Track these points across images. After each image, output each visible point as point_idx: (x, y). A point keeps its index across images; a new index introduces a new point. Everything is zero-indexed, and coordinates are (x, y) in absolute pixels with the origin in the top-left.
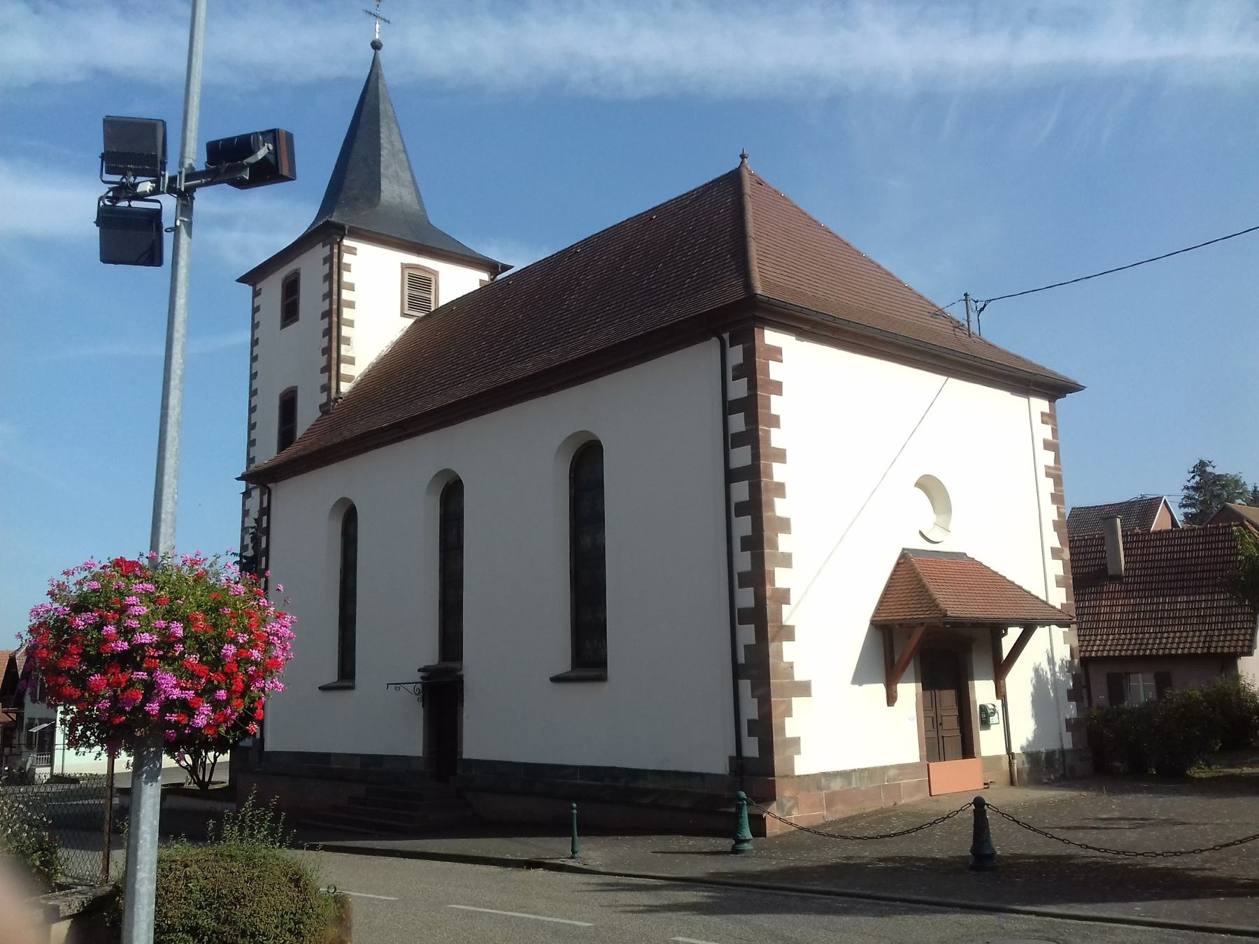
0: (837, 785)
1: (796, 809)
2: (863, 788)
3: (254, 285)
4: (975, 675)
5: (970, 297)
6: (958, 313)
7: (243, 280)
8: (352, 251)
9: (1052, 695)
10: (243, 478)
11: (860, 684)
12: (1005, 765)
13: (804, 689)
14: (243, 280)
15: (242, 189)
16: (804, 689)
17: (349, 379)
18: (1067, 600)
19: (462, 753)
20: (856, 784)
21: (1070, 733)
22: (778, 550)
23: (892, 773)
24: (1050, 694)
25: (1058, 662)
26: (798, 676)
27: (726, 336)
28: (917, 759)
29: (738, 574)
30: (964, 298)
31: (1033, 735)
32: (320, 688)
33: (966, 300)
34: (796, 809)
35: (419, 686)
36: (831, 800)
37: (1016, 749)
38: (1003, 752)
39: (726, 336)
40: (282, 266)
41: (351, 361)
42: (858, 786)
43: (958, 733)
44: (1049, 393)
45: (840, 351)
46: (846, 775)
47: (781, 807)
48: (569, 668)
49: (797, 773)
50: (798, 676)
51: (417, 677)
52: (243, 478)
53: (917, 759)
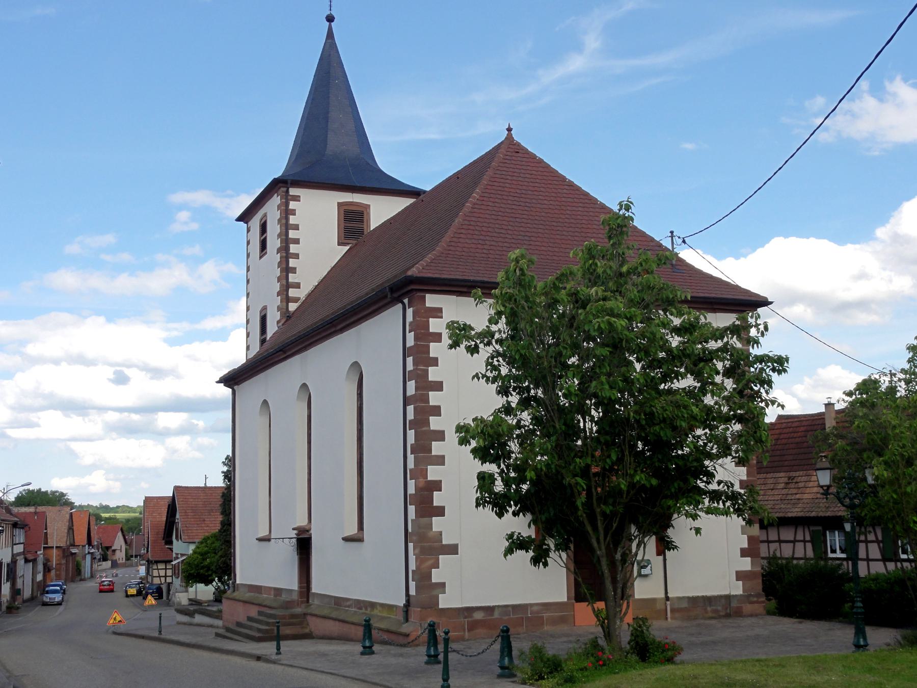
0: (478, 616)
3: (246, 223)
5: (674, 234)
6: (667, 243)
7: (239, 219)
8: (297, 198)
14: (239, 219)
17: (296, 300)
18: (747, 477)
19: (278, 591)
21: (740, 583)
23: (535, 608)
27: (406, 301)
29: (410, 470)
30: (670, 235)
32: (257, 539)
33: (672, 237)
35: (294, 540)
38: (662, 595)
39: (406, 301)
40: (260, 209)
41: (297, 286)
48: (356, 532)
51: (293, 534)
53: (565, 600)
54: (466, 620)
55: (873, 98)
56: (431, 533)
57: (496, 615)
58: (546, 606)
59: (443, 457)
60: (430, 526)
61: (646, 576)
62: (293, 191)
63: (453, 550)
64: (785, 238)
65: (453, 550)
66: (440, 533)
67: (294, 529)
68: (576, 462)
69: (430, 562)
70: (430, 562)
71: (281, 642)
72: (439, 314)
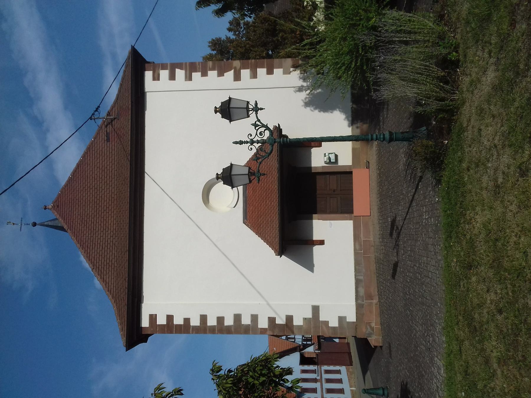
0: (362, 291)
1: (371, 324)
2: (364, 270)
4: (309, 166)
9: (320, 90)
10: (229, 32)
11: (313, 266)
12: (358, 144)
13: (302, 106)
15: (146, 110)
16: (302, 106)
20: (362, 276)
22: (249, 325)
24: (320, 92)
25: (300, 83)
26: (309, 315)
28: (351, 222)
31: (342, 113)
34: (371, 324)
36: (369, 297)
37: (348, 131)
42: (363, 274)
43: (338, 175)
44: (140, 136)
45: (146, 138)
46: (358, 282)
47: (370, 335)
49: (355, 321)
50: (309, 315)
52: (229, 32)
53: (351, 222)
54: (364, 301)
55: (131, 48)
56: (304, 326)
57: (361, 278)
58: (356, 237)
59: (252, 316)
60: (299, 327)
61: (336, 156)
62: (145, 323)
63: (316, 309)
64: (222, 103)
65: (316, 309)
66: (305, 319)
67: (279, 125)
68: (302, 64)
69: (324, 327)
70: (324, 327)
71: (315, 238)
72: (154, 316)
